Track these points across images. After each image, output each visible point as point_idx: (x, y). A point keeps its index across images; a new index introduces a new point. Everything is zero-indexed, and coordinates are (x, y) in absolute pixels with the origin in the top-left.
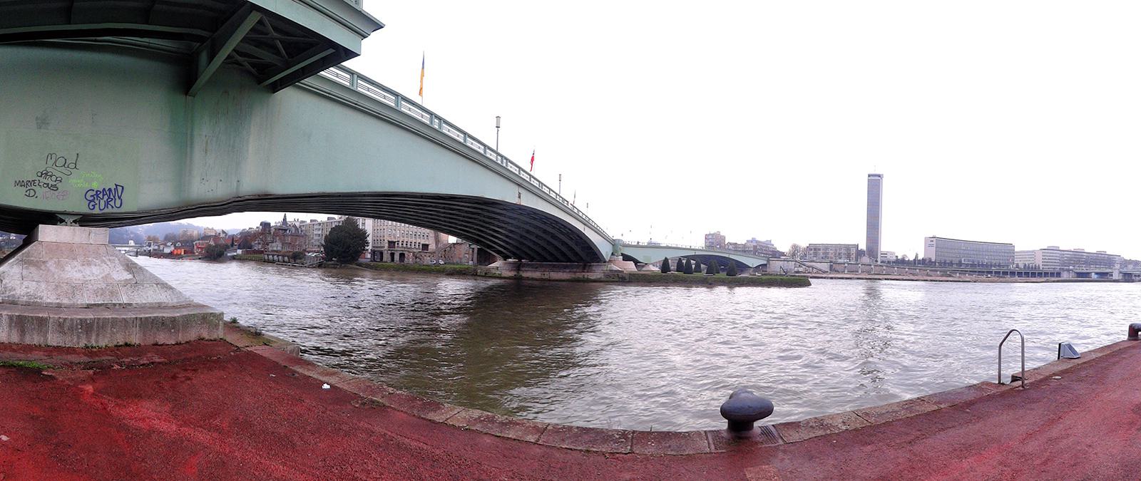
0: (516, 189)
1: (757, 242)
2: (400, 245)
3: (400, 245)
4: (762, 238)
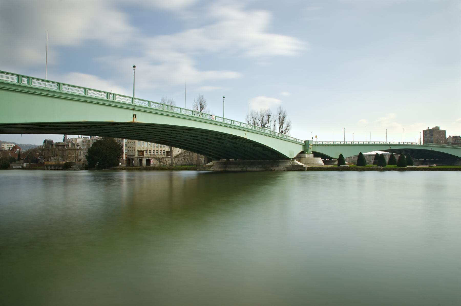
0: (131, 113)
2: (148, 153)
3: (148, 153)
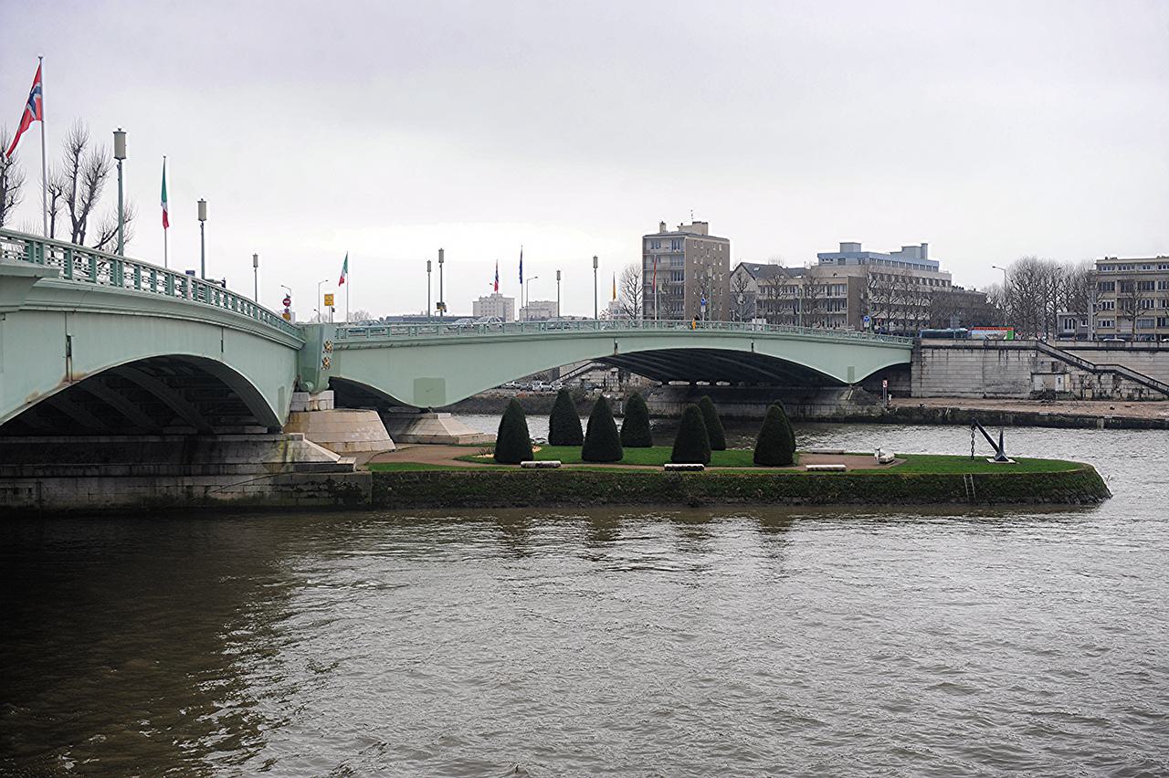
0: (611, 343)
1: (864, 259)
4: (881, 241)
